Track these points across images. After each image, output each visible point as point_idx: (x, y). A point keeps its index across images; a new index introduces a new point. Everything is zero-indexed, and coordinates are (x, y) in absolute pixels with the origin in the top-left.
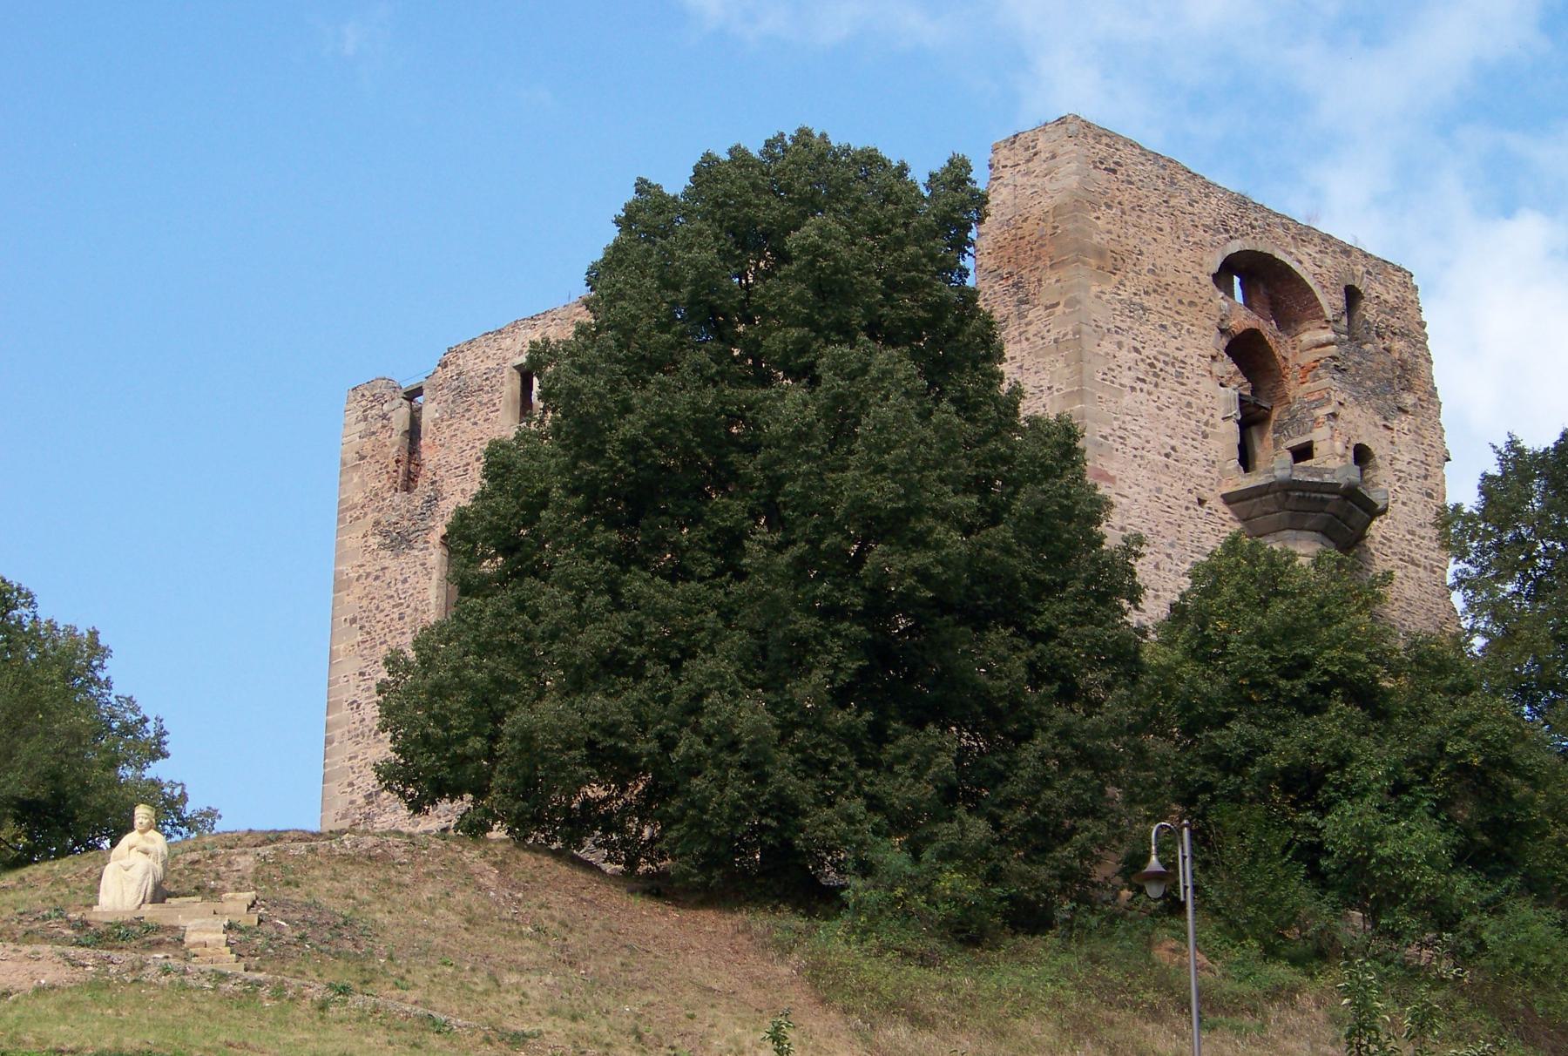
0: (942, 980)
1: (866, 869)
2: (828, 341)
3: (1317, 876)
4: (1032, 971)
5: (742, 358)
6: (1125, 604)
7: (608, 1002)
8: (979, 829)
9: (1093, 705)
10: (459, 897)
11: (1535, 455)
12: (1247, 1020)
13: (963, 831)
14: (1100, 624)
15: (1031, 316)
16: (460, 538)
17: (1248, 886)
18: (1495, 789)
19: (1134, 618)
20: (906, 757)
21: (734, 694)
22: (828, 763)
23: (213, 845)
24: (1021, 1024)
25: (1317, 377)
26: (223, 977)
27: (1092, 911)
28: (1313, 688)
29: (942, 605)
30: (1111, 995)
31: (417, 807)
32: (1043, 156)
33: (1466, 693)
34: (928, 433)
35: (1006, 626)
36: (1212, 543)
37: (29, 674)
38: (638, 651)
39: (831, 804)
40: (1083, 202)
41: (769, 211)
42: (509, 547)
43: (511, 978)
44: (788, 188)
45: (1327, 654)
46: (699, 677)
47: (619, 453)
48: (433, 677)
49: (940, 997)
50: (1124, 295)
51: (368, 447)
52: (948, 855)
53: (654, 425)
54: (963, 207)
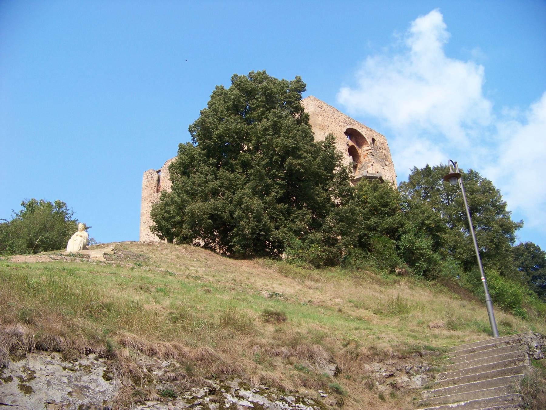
14: (344, 185)
22: (277, 218)
25: (368, 157)
47: (216, 138)
51: (148, 184)
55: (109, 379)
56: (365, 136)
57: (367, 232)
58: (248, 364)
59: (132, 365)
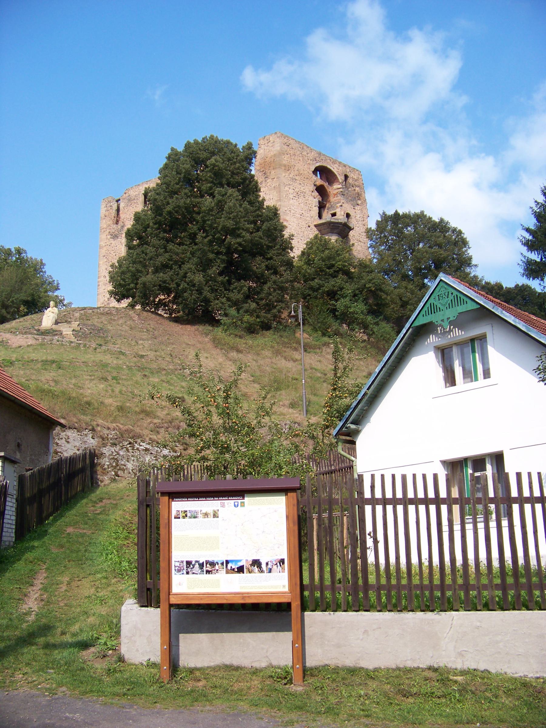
0: (245, 341)
1: (226, 315)
2: (217, 187)
3: (336, 317)
4: (267, 339)
5: (197, 191)
6: (289, 251)
7: (164, 347)
8: (253, 305)
9: (281, 275)
10: (128, 323)
11: (389, 216)
12: (318, 351)
13: (250, 306)
14: (283, 256)
15: (268, 181)
16: (130, 235)
17: (318, 319)
18: (378, 296)
19: (292, 255)
20: (236, 288)
21: (194, 273)
22: (217, 289)
23: (70, 311)
24: (263, 352)
25: (337, 196)
26: (72, 342)
27: (281, 325)
28: (335, 271)
29: (244, 251)
30: (284, 344)
31: (118, 301)
32: (271, 142)
33: (371, 273)
34: (241, 209)
35: (260, 256)
36: (312, 236)
37: (25, 270)
38: (171, 263)
39: (218, 300)
40: (281, 153)
41: (203, 155)
42: (140, 238)
43: (141, 342)
44: (208, 150)
45: (338, 263)
46: (186, 269)
48: (122, 269)
49: (244, 345)
50: (291, 176)
52: (246, 311)
53: (175, 208)
54: (251, 154)
55: (93, 439)
56: (336, 173)
57: (310, 293)
58: (146, 432)
59: (101, 434)
